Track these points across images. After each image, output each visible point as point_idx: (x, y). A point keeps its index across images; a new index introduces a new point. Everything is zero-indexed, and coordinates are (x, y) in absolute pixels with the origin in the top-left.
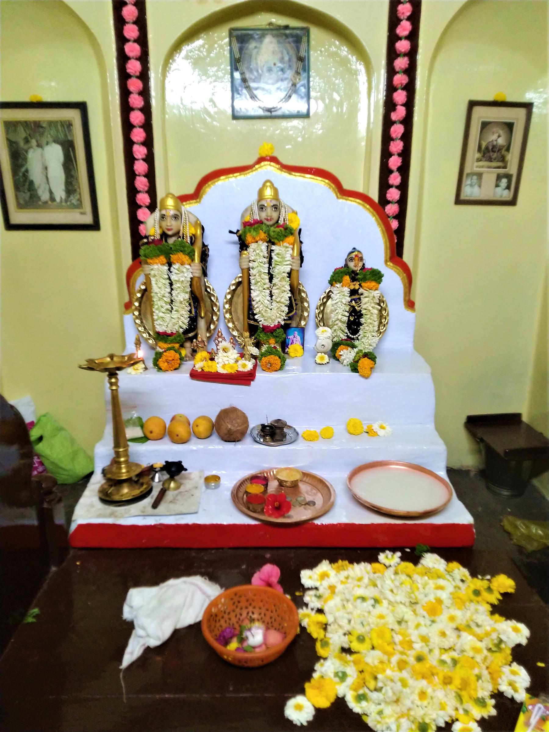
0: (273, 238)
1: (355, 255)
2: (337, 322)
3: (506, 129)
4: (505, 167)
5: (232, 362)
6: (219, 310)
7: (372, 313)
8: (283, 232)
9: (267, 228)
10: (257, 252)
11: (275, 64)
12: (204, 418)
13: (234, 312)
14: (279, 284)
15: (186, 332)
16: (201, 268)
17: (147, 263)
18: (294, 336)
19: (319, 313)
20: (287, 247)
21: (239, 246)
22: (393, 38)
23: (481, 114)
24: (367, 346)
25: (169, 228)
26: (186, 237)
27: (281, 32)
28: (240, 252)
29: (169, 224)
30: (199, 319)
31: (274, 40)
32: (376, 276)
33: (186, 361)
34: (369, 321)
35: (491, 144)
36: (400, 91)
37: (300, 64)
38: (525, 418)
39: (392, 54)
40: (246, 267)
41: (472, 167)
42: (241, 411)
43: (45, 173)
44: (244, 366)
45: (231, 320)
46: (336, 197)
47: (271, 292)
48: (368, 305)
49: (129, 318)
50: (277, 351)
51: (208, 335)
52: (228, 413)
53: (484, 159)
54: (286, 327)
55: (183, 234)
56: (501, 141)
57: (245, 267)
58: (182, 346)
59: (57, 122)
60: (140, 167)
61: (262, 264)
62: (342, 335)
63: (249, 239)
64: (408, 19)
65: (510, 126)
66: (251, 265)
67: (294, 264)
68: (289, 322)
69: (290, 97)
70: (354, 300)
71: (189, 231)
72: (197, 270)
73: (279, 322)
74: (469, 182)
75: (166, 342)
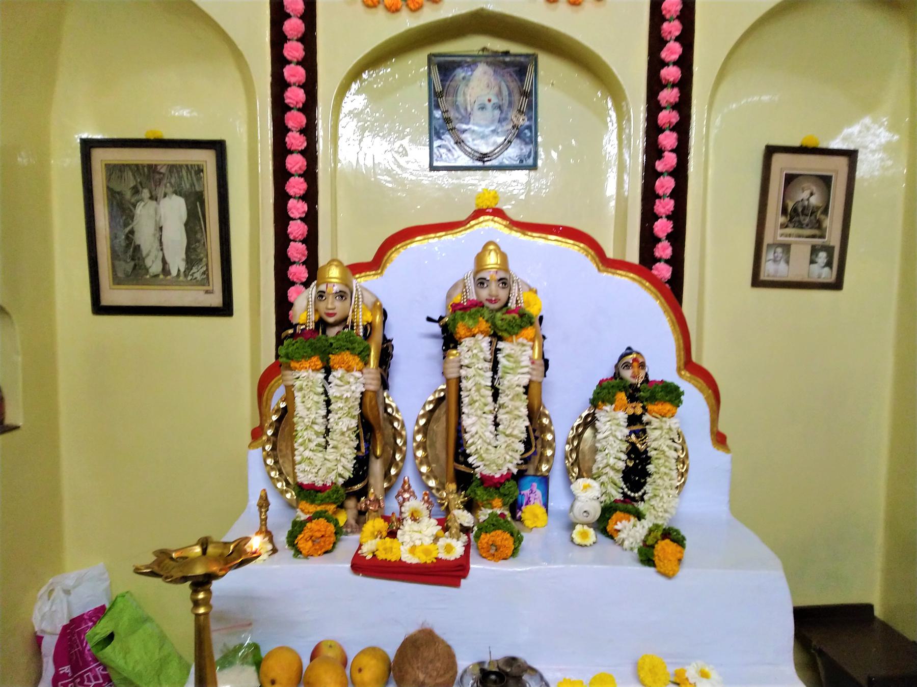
0: (502, 331)
1: (629, 358)
2: (608, 469)
3: (821, 182)
4: (822, 236)
5: (428, 541)
6: (405, 443)
7: (668, 457)
8: (518, 321)
9: (489, 314)
10: (475, 351)
11: (489, 101)
12: (373, 651)
13: (430, 446)
14: (511, 405)
15: (349, 483)
16: (379, 376)
17: (289, 368)
18: (531, 490)
19: (571, 450)
20: (523, 345)
21: (442, 341)
22: (655, 64)
23: (782, 164)
24: (660, 514)
25: (331, 312)
26: (358, 326)
27: (498, 61)
28: (444, 351)
29: (330, 306)
30: (373, 459)
31: (490, 70)
32: (672, 394)
33: (347, 533)
34: (663, 469)
35: (800, 204)
36: (667, 132)
37: (525, 102)
38: (878, 612)
39: (655, 84)
40: (455, 375)
41: (775, 237)
42: (443, 642)
43: (158, 235)
44: (449, 548)
45: (425, 460)
46: (596, 270)
47: (496, 417)
48: (657, 439)
49: (256, 455)
50: (506, 521)
51: (386, 485)
52: (418, 649)
53: (790, 225)
54: (519, 477)
55: (352, 322)
56: (815, 201)
57: (452, 374)
58: (341, 506)
59: (181, 166)
60: (297, 229)
61: (481, 372)
62: (614, 492)
63: (461, 330)
64: (677, 39)
65: (826, 181)
66: (463, 372)
67: (535, 373)
68: (524, 467)
69: (510, 142)
70: (634, 432)
71: (363, 317)
72: (373, 379)
73: (509, 469)
74: (771, 256)
75: (313, 502)
